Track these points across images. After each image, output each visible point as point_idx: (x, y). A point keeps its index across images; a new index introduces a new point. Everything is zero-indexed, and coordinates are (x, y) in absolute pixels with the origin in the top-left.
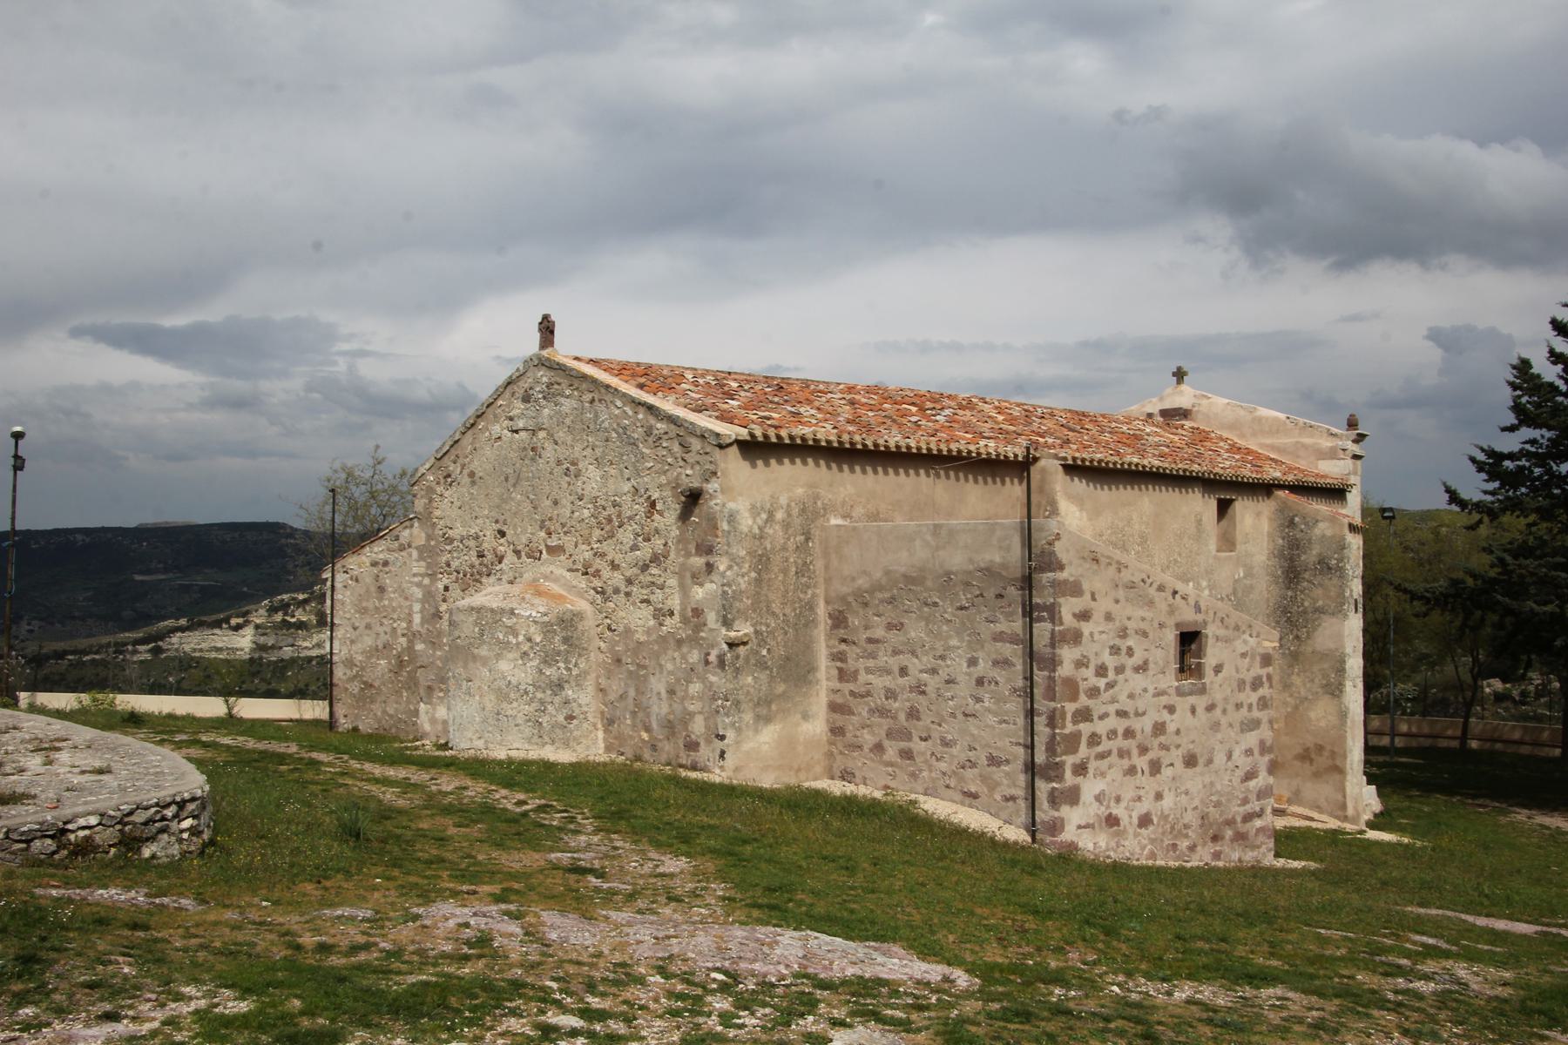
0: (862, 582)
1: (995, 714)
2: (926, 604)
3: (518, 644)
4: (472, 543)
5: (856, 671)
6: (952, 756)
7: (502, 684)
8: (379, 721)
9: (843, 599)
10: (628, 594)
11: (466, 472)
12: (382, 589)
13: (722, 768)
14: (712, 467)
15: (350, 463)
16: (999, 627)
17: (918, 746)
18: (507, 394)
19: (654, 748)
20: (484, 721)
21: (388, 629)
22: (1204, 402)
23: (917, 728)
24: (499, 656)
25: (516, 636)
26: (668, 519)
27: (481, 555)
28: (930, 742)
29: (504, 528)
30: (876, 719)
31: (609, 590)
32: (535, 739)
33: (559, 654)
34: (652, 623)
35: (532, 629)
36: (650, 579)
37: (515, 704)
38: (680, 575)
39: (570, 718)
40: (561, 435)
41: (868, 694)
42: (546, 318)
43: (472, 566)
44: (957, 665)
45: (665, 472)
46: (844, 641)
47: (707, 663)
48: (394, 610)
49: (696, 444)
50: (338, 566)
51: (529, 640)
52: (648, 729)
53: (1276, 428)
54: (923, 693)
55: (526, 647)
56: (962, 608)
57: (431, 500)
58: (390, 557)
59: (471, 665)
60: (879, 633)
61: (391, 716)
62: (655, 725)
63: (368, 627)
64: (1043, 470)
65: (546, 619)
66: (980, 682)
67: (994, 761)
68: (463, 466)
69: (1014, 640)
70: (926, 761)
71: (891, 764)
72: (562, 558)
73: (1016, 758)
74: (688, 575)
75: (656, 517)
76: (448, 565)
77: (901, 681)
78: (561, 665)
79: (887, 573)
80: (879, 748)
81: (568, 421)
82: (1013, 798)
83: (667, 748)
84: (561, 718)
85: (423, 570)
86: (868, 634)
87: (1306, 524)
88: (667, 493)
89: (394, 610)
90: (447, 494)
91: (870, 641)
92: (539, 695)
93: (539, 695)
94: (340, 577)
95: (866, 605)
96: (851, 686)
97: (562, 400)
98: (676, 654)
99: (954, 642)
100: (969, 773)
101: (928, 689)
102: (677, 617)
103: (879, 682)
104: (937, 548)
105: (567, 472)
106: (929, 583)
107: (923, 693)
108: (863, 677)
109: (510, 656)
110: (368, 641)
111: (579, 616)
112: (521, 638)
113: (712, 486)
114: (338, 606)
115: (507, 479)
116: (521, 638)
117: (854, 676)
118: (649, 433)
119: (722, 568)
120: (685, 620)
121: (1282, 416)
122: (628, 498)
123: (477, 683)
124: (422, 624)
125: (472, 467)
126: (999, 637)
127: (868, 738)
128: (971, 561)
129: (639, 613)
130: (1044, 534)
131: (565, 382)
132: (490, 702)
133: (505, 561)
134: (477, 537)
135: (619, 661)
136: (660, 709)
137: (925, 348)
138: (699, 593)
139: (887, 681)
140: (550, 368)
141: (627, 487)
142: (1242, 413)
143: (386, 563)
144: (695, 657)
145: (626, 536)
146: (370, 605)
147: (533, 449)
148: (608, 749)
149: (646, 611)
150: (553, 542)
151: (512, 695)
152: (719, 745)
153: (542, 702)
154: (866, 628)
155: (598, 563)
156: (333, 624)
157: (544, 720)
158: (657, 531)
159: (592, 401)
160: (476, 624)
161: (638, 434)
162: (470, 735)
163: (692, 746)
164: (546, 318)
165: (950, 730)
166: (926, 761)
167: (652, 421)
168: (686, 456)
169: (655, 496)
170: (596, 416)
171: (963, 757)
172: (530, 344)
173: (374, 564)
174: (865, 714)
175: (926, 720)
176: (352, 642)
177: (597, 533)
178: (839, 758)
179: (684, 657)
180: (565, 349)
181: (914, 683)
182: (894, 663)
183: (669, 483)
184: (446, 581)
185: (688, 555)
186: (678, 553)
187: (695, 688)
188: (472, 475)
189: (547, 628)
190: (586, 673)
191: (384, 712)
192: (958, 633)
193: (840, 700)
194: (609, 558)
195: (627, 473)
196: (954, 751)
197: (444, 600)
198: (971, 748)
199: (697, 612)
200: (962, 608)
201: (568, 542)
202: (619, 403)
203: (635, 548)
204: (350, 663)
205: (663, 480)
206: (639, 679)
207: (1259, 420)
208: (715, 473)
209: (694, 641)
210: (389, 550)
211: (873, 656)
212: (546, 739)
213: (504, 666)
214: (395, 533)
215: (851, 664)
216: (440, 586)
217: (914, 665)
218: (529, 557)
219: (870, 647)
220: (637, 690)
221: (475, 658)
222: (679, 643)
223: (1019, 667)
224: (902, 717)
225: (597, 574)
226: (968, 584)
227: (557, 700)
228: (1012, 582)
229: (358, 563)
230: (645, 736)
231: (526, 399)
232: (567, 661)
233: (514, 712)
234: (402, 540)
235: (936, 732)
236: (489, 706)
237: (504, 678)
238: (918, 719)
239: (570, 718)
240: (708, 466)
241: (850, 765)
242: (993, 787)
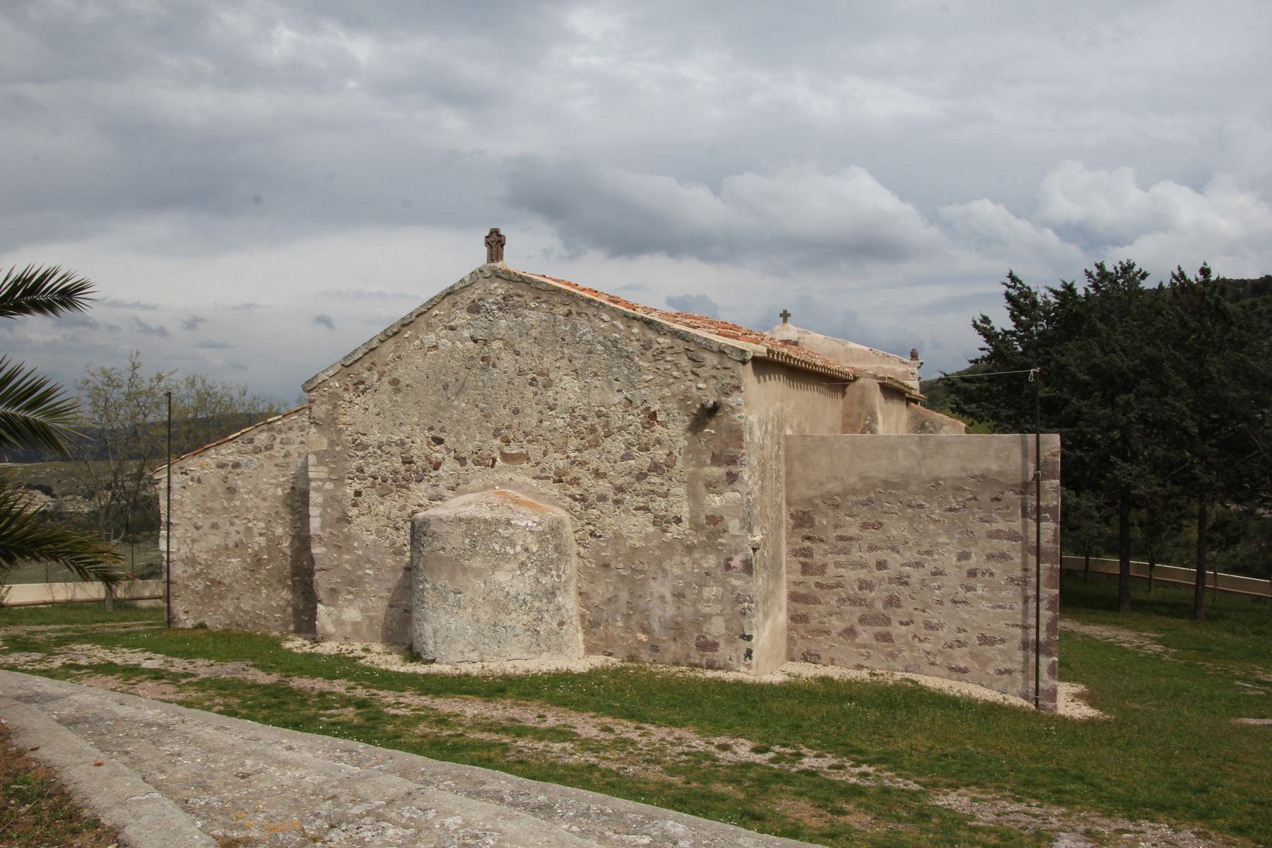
0: (834, 487)
1: (989, 600)
2: (909, 506)
3: (516, 555)
4: (395, 449)
5: (824, 566)
6: (938, 638)
7: (500, 595)
8: (231, 617)
9: (810, 501)
10: (617, 502)
11: (385, 379)
12: (232, 491)
13: (749, 666)
14: (735, 382)
15: (108, 366)
16: (995, 527)
17: (896, 629)
18: (446, 303)
19: (655, 648)
20: (480, 633)
21: (241, 529)
22: (807, 336)
23: (896, 615)
24: (495, 568)
25: (514, 547)
26: (675, 431)
27: (408, 461)
28: (912, 627)
29: (442, 436)
30: (847, 608)
31: (592, 498)
32: (534, 648)
33: (552, 562)
34: (651, 529)
35: (529, 539)
36: (648, 487)
37: (514, 615)
38: (691, 484)
39: (561, 624)
40: (524, 345)
41: (838, 585)
42: (495, 232)
43: (396, 472)
44: (947, 559)
45: (668, 386)
46: (809, 538)
47: (728, 567)
48: (248, 510)
49: (711, 359)
50: (175, 467)
51: (527, 550)
52: (645, 631)
53: (863, 358)
54: (906, 584)
55: (523, 558)
56: (951, 510)
57: (335, 406)
58: (243, 459)
59: (460, 577)
60: (853, 531)
61: (247, 613)
62: (656, 626)
63: (214, 526)
64: (863, 387)
65: (540, 528)
66: (972, 573)
67: (985, 640)
68: (382, 374)
69: (1012, 536)
70: (907, 643)
71: (865, 646)
72: (525, 465)
73: (1013, 637)
74: (701, 484)
75: (658, 428)
76: (360, 470)
77: (878, 574)
78: (554, 573)
79: (863, 478)
80: (850, 632)
81: (534, 333)
82: (1009, 672)
83: (674, 649)
84: (555, 625)
85: (324, 475)
86: (839, 532)
87: (934, 427)
88: (672, 405)
89: (248, 510)
90: (357, 400)
91: (841, 538)
92: (537, 604)
93: (537, 604)
94: (177, 479)
95: (837, 506)
96: (818, 579)
97: (526, 312)
98: (686, 560)
99: (943, 539)
100: (957, 652)
101: (912, 580)
102: (686, 524)
103: (851, 575)
104: (924, 458)
105: (533, 382)
106: (913, 488)
107: (906, 584)
108: (831, 570)
109: (508, 567)
110: (215, 540)
111: (560, 522)
112: (518, 548)
113: (732, 400)
114: (174, 507)
115: (446, 387)
116: (518, 548)
117: (822, 569)
118: (647, 346)
119: (746, 478)
120: (696, 527)
121: (867, 349)
122: (620, 409)
123: (469, 595)
124: (323, 528)
125: (395, 375)
126: (996, 535)
127: (837, 624)
128: (963, 469)
129: (634, 520)
130: (1048, 447)
131: (528, 296)
132: (485, 614)
133: (443, 467)
134: (402, 444)
135: (606, 566)
136: (662, 611)
137: (569, 284)
138: (715, 502)
139: (862, 574)
140: (509, 280)
141: (617, 398)
142: (837, 345)
143: (236, 465)
144: (711, 561)
145: (616, 445)
146: (217, 505)
147: (483, 359)
148: (590, 650)
149: (643, 519)
150: (513, 449)
151: (511, 606)
152: (744, 645)
153: (539, 611)
154: (836, 527)
155: (576, 471)
156: (169, 523)
157: (542, 628)
158: (659, 442)
159: (569, 314)
160: (466, 535)
161: (634, 347)
162: (460, 647)
163: (707, 646)
164: (495, 232)
165: (934, 616)
166: (907, 643)
167: (651, 335)
168: (699, 371)
169: (655, 407)
170: (575, 328)
171: (951, 638)
172: (480, 257)
173: (221, 466)
174: (833, 602)
175: (908, 607)
176: (194, 541)
177: (574, 442)
178: (800, 642)
179: (695, 562)
180: (512, 261)
181: (894, 575)
182: (871, 558)
183: (674, 396)
184: (357, 486)
185: (701, 464)
186: (687, 462)
187: (712, 591)
188: (395, 382)
189: (541, 538)
190: (570, 578)
191: (238, 608)
192: (947, 532)
193: (802, 590)
194: (592, 466)
195: (617, 385)
196: (941, 633)
197: (355, 505)
198: (959, 630)
199: (714, 519)
200: (951, 510)
201: (535, 450)
202: (606, 317)
203: (627, 457)
204: (191, 561)
205: (667, 392)
206: (635, 581)
207: (851, 350)
208: (738, 388)
209: (711, 545)
210: (240, 452)
211: (845, 552)
212: (543, 647)
213: (501, 577)
214: (249, 436)
215: (818, 559)
216: (350, 491)
217: (894, 561)
218: (477, 463)
219: (841, 544)
220: (632, 594)
221: (465, 570)
222: (689, 549)
223: (1018, 560)
224: (879, 605)
225: (575, 481)
226: (959, 489)
227: (551, 607)
228: (1011, 487)
229: (204, 464)
230: (643, 637)
231: (474, 309)
232: (558, 569)
233: (513, 623)
234: (257, 443)
235: (919, 617)
236: (484, 618)
237: (502, 589)
238: (899, 606)
239: (561, 624)
240: (728, 380)
241: (814, 647)
242: (984, 663)
